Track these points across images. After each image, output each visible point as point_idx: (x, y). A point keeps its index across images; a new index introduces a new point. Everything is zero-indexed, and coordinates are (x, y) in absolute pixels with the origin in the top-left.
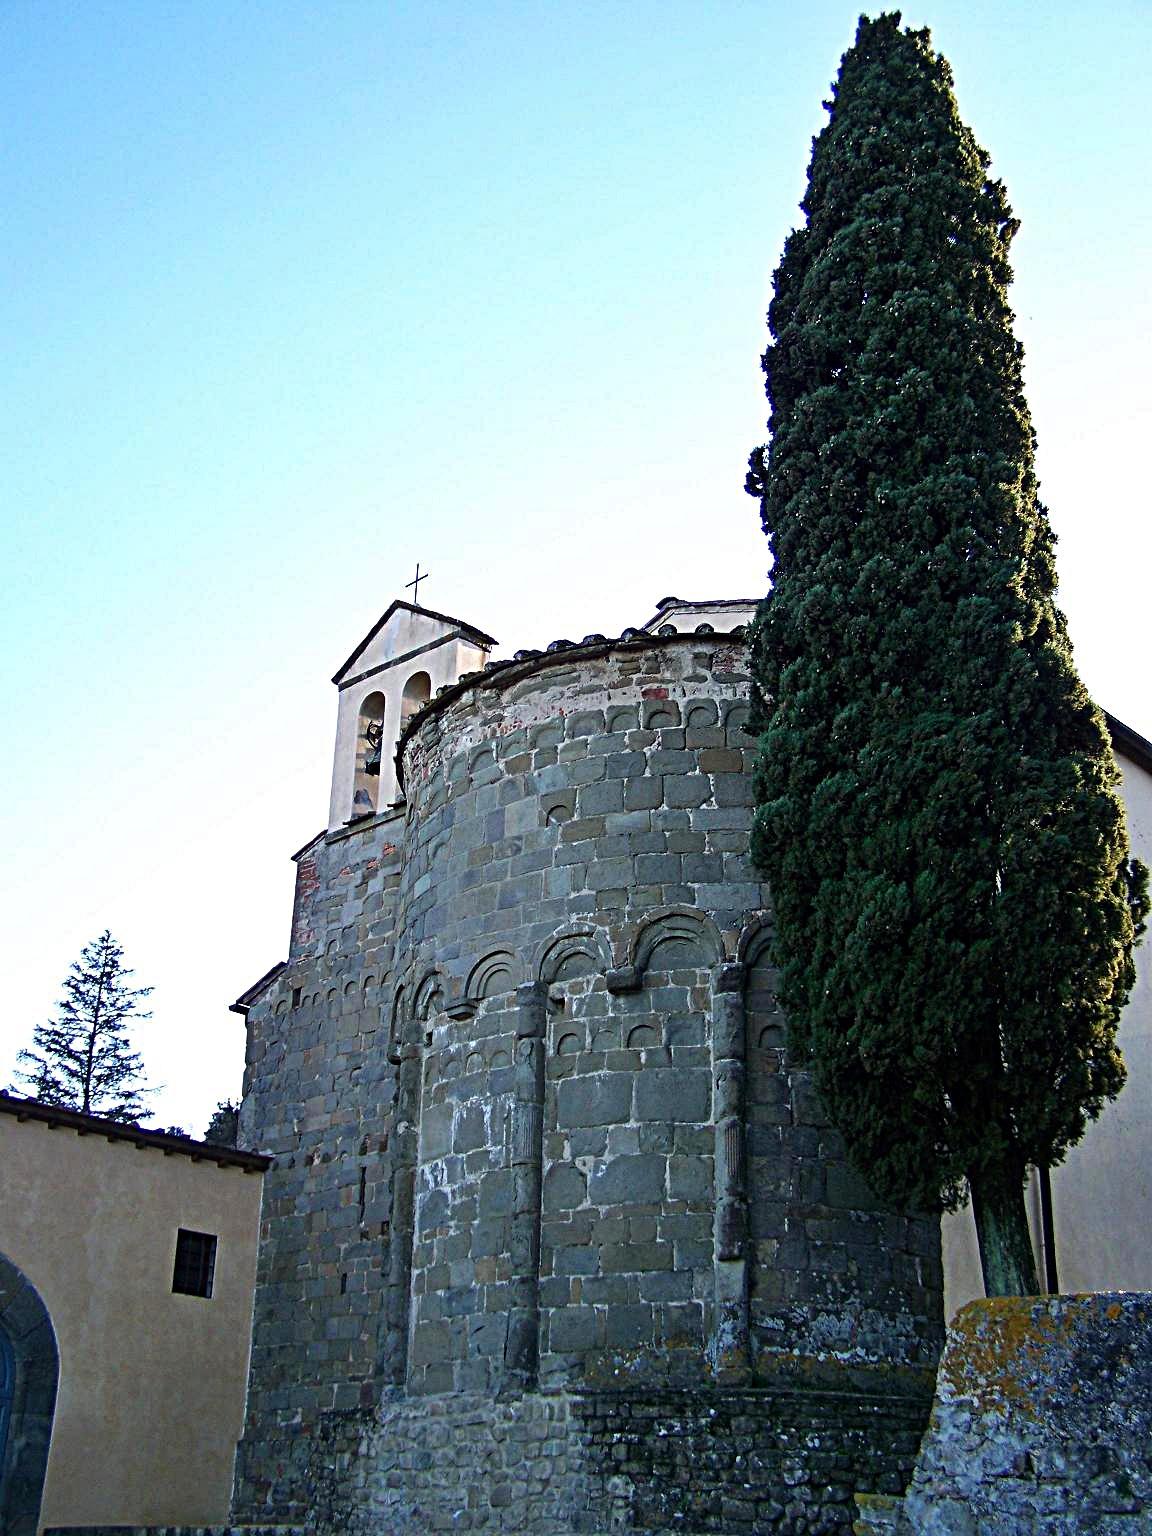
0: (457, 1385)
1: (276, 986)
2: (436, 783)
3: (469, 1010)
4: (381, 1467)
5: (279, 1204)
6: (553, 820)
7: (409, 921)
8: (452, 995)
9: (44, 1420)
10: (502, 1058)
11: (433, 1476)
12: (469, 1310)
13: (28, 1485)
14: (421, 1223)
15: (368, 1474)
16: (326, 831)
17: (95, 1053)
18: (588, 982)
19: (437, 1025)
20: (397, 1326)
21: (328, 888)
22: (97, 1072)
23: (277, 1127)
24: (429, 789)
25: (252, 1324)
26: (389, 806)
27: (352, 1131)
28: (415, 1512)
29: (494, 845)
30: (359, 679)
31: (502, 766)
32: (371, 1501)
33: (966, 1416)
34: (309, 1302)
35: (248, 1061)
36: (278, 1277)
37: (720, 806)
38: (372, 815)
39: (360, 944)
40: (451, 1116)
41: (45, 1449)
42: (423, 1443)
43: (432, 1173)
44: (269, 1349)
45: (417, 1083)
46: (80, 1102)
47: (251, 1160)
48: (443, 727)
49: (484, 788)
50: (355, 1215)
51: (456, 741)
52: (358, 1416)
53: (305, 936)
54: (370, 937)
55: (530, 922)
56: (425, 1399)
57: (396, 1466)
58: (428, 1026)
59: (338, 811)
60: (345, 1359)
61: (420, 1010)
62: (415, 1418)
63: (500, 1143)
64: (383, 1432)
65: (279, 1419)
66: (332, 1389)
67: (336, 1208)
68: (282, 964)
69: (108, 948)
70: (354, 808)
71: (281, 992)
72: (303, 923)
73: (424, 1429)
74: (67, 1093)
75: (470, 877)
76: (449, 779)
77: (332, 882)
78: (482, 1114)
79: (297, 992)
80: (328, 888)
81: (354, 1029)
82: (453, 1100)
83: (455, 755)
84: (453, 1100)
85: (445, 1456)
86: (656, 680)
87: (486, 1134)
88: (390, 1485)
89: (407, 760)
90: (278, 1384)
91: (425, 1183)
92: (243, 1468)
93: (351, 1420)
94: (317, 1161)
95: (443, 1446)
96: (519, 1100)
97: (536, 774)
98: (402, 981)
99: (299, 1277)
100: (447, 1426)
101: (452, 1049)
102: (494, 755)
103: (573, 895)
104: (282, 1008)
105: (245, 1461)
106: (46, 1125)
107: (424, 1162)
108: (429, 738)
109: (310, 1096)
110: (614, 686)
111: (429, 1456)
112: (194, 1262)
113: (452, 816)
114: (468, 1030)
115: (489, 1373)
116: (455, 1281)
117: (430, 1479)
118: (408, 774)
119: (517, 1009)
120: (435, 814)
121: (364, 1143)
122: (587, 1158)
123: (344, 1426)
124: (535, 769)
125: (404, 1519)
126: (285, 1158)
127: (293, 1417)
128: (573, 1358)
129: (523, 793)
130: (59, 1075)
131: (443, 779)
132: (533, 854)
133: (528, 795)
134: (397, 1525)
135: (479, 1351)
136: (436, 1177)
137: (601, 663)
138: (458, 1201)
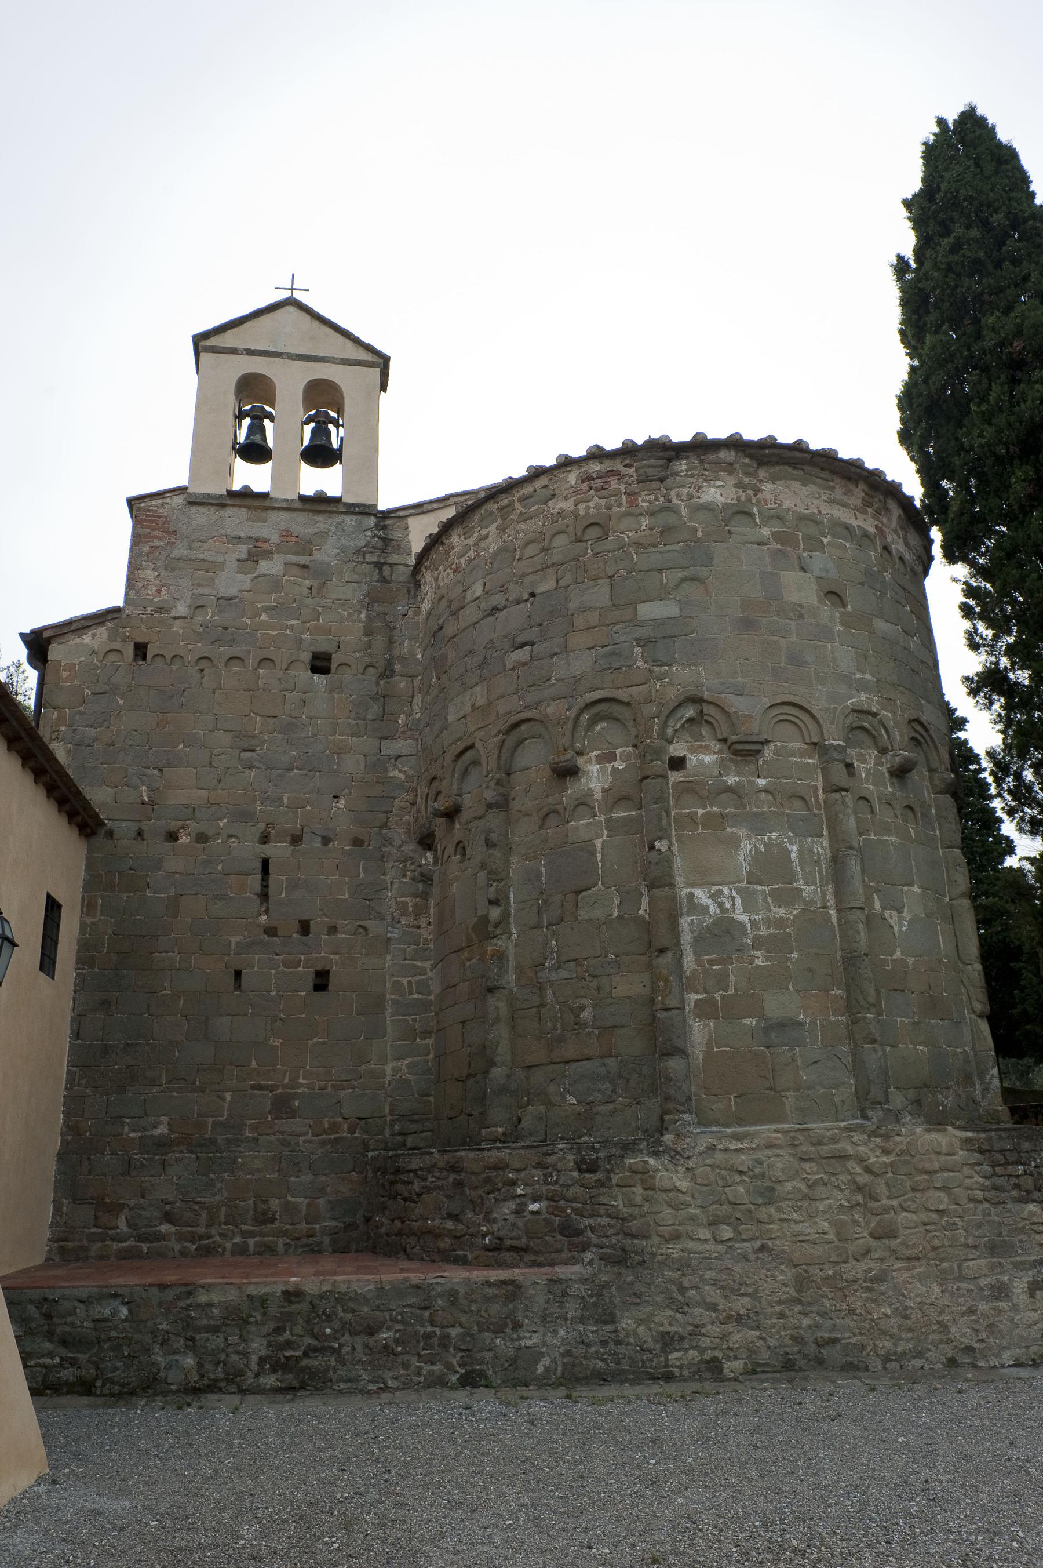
30: (234, 351)
61: (670, 731)
62: (737, 1150)
63: (814, 883)
65: (126, 1129)
94: (184, 840)
103: (858, 676)
110: (855, 509)
128: (911, 1094)
137: (852, 487)
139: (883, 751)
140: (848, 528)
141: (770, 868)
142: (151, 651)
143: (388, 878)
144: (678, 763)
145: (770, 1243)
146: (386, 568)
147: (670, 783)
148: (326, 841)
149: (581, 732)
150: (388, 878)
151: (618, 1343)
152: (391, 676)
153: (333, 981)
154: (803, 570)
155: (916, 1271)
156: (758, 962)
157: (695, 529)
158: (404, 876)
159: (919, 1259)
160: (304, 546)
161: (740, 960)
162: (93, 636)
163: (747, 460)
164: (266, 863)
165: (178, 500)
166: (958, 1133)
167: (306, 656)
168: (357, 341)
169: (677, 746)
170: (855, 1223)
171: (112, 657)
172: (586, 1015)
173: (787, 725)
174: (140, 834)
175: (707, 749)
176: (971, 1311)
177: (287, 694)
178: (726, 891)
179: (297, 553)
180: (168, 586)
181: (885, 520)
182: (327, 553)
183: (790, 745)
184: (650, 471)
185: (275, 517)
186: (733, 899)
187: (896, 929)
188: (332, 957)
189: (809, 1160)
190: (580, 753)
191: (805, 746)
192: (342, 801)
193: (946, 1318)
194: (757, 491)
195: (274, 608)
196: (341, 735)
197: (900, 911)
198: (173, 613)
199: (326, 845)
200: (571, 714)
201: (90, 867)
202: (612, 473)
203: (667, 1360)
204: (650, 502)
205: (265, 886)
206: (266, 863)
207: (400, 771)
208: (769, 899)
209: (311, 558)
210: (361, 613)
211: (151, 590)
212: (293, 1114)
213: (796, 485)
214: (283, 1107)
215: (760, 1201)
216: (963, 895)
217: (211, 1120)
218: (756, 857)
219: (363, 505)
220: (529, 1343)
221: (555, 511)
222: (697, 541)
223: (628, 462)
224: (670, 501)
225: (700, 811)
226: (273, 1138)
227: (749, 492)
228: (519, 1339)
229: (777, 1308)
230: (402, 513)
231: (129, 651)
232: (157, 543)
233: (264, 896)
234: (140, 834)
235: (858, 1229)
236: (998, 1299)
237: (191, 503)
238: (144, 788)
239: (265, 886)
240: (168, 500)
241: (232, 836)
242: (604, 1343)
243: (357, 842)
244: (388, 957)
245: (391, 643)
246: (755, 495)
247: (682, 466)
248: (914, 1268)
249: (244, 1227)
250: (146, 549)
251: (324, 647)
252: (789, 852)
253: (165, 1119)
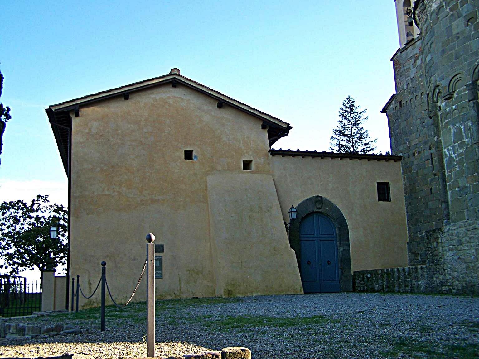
0: (466, 217)
1: (393, 102)
2: (427, 22)
3: (450, 96)
4: (446, 245)
5: (407, 169)
6: (470, 24)
7: (427, 71)
8: (444, 92)
9: (347, 242)
10: (465, 109)
11: (463, 247)
12: (466, 193)
13: (346, 261)
14: (447, 168)
15: (443, 248)
16: (399, 49)
17: (353, 134)
19: (441, 103)
20: (445, 202)
21: (404, 67)
22: (355, 139)
23: (402, 146)
24: (425, 25)
25: (405, 207)
26: (418, 35)
27: (426, 143)
28: (459, 258)
29: (450, 38)
31: (448, 10)
32: (445, 256)
34: (421, 198)
35: (389, 127)
36: (410, 192)
38: (413, 39)
39: (417, 82)
40: (451, 132)
41: (349, 251)
42: (458, 237)
43: (448, 151)
44: (412, 214)
45: (438, 123)
46: (352, 149)
47: (396, 158)
48: (425, 3)
49: (443, 20)
50: (431, 169)
51: (431, 6)
52: (437, 231)
53: (400, 84)
54: (420, 79)
55: (466, 61)
56: (457, 223)
57: (451, 245)
58: (439, 104)
59: (402, 41)
60: (435, 214)
61: (435, 99)
64: (445, 235)
66: (433, 224)
67: (425, 168)
68: (394, 95)
69: (350, 101)
70: (407, 39)
71: (395, 104)
72: (398, 80)
73: (458, 232)
74: (347, 148)
75: (443, 51)
76: (431, 20)
77: (405, 65)
78: (461, 129)
79: (400, 102)
80: (404, 67)
81: (419, 109)
82: (450, 127)
83: (431, 11)
84: (450, 127)
85: (466, 240)
87: (463, 136)
88: (450, 251)
89: (417, 18)
90: (416, 224)
91: (446, 155)
92: (410, 250)
93: (435, 232)
94: (416, 154)
95: (465, 237)
96: (472, 122)
97: (461, 9)
98: (428, 91)
99: (417, 191)
100: (465, 231)
101: (447, 110)
102: (445, 7)
104: (397, 108)
105: (410, 248)
106: (291, 156)
107: (445, 148)
108: (422, 8)
109: (411, 134)
111: (461, 241)
112: (383, 191)
113: (434, 33)
114: (452, 102)
115: (476, 213)
116: (461, 185)
117: (462, 247)
118: (418, 22)
119: (467, 92)
120: (428, 33)
121: (430, 146)
123: (433, 234)
125: (456, 261)
126: (406, 155)
127: (423, 233)
129: (457, 17)
130: (343, 143)
131: (429, 21)
132: (464, 38)
133: (459, 17)
134: (454, 262)
135: (472, 206)
136: (449, 153)
138: (457, 159)
173: (457, 84)
203: (442, 289)
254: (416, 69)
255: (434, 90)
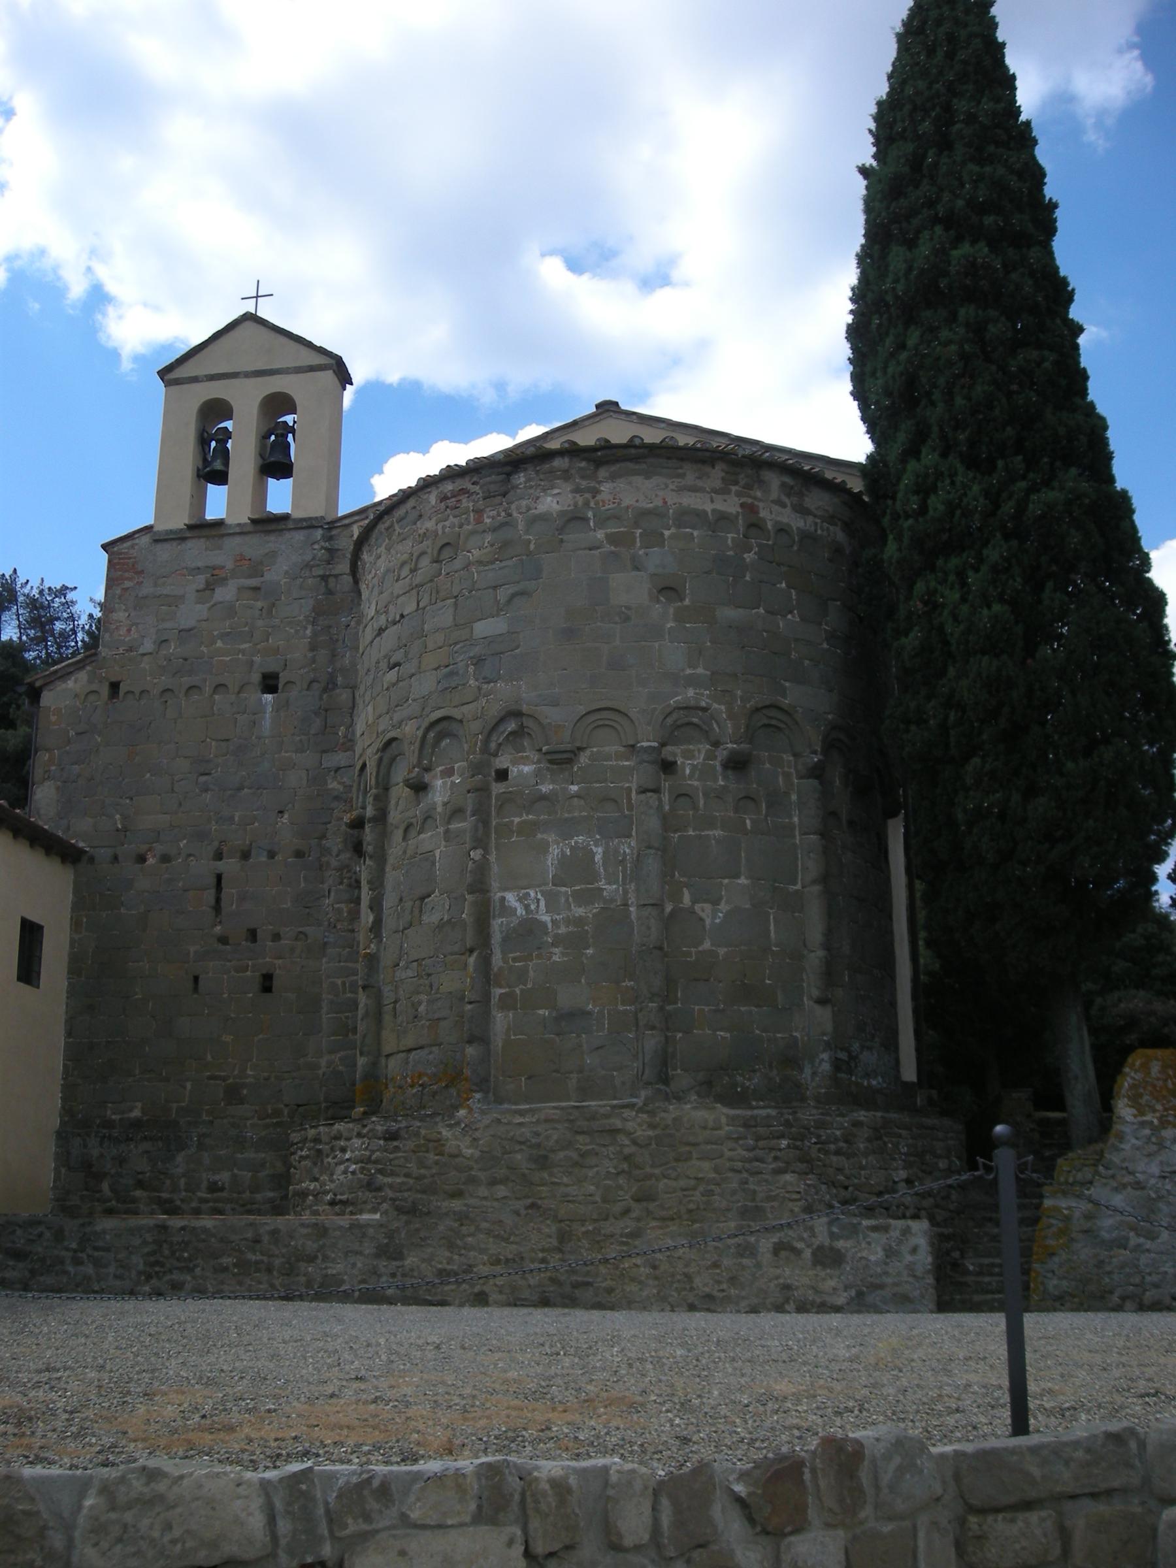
18: (699, 751)
30: (195, 380)
33: (1147, 1132)
37: (802, 620)
54: (219, 644)
61: (493, 745)
63: (616, 882)
65: (109, 1113)
78: (592, 854)
86: (750, 497)
94: (151, 861)
103: (688, 671)
110: (716, 491)
122: (705, 905)
124: (641, 548)
127: (131, 1110)
137: (708, 469)
139: (716, 744)
140: (700, 514)
141: (577, 868)
142: (123, 688)
143: (326, 886)
144: (502, 775)
145: (539, 1202)
146: (332, 580)
147: (494, 793)
148: (272, 855)
149: (428, 750)
150: (326, 886)
151: (404, 1275)
152: (333, 689)
153: (276, 983)
154: (638, 569)
155: (668, 1230)
156: (556, 958)
157: (529, 541)
158: (341, 883)
159: (673, 1219)
160: (256, 569)
161: (539, 956)
162: (76, 682)
163: (583, 464)
164: (219, 878)
165: (145, 540)
166: (725, 1110)
167: (256, 678)
168: (309, 345)
169: (502, 758)
170: (620, 1187)
171: (92, 698)
172: (422, 1009)
174: (116, 858)
175: (525, 761)
176: (716, 1265)
177: (237, 716)
178: (532, 894)
179: (250, 577)
180: (137, 624)
181: (759, 494)
182: (276, 574)
183: (607, 749)
184: (493, 487)
185: (233, 544)
186: (538, 900)
187: (708, 922)
188: (276, 961)
189: (583, 1133)
190: (427, 770)
191: (622, 749)
192: (286, 816)
193: (692, 1270)
194: (595, 492)
195: (228, 634)
196: (286, 752)
197: (716, 902)
198: (141, 651)
199: (273, 857)
200: (420, 733)
201: (76, 891)
202: (463, 491)
204: (493, 518)
205: (218, 900)
206: (219, 878)
207: (339, 783)
208: (571, 899)
209: (262, 579)
210: (306, 628)
211: (123, 631)
212: (242, 1102)
213: (638, 480)
214: (233, 1094)
215: (533, 1166)
216: (814, 882)
217: (175, 1105)
218: (563, 861)
219: (310, 519)
220: (334, 1272)
221: (421, 532)
222: (529, 554)
223: (475, 479)
224: (510, 515)
225: (517, 820)
226: (225, 1121)
227: (588, 495)
228: (326, 1268)
229: (540, 1255)
230: (347, 521)
231: (105, 691)
232: (127, 584)
233: (217, 907)
234: (116, 858)
235: (621, 1193)
236: (742, 1256)
237: (156, 541)
238: (118, 816)
239: (218, 900)
240: (137, 541)
241: (190, 855)
242: (393, 1275)
243: (299, 854)
244: (324, 960)
245: (334, 656)
246: (594, 497)
247: (520, 479)
248: (668, 1226)
249: (199, 1194)
250: (118, 592)
251: (273, 666)
252: (593, 854)
253: (139, 1105)
254: (210, 609)
255: (502, 720)
